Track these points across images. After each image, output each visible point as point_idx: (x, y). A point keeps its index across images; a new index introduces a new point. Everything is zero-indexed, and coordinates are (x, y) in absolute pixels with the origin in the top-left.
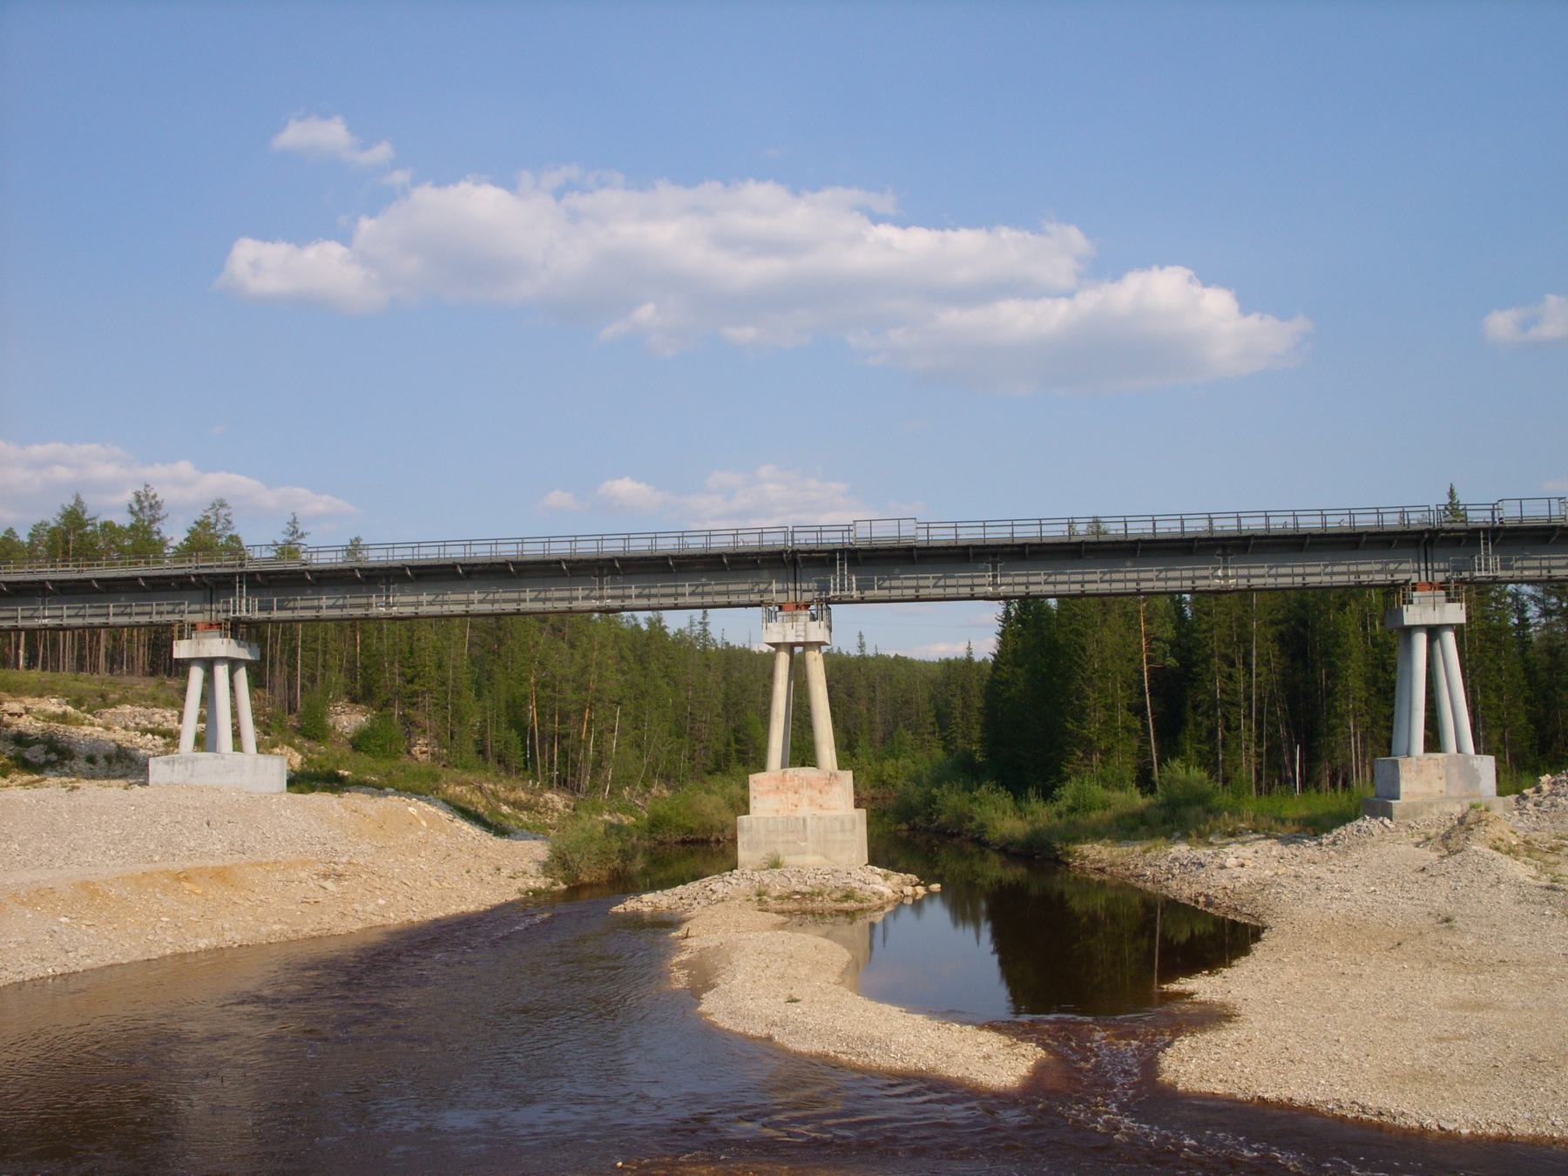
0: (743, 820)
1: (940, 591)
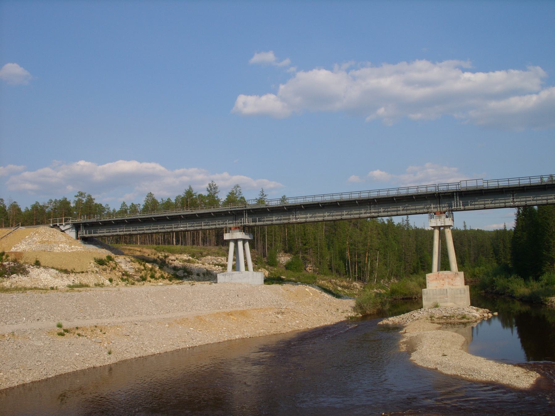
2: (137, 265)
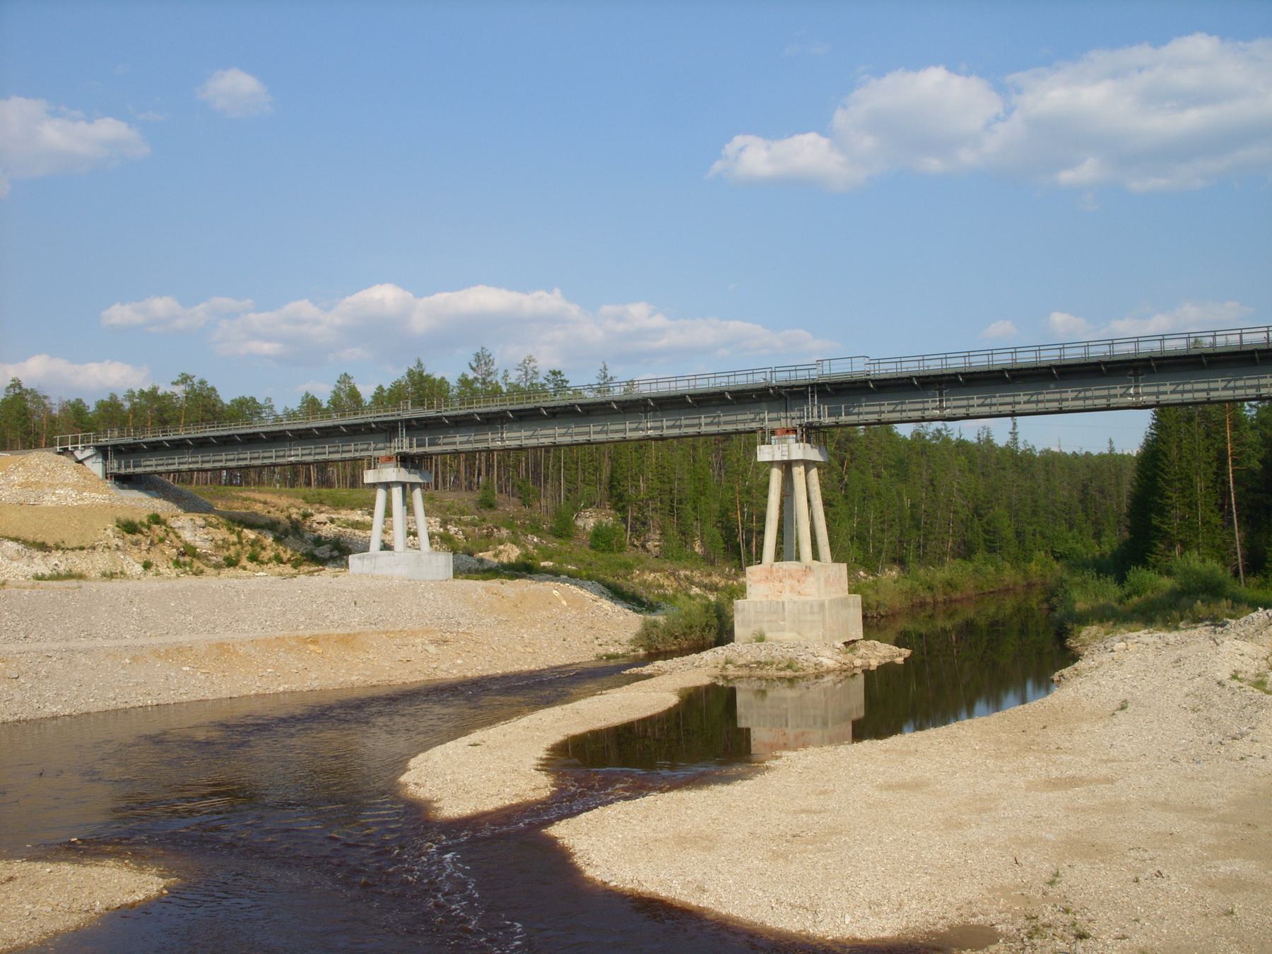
0: (739, 603)
1: (1080, 403)
2: (221, 534)
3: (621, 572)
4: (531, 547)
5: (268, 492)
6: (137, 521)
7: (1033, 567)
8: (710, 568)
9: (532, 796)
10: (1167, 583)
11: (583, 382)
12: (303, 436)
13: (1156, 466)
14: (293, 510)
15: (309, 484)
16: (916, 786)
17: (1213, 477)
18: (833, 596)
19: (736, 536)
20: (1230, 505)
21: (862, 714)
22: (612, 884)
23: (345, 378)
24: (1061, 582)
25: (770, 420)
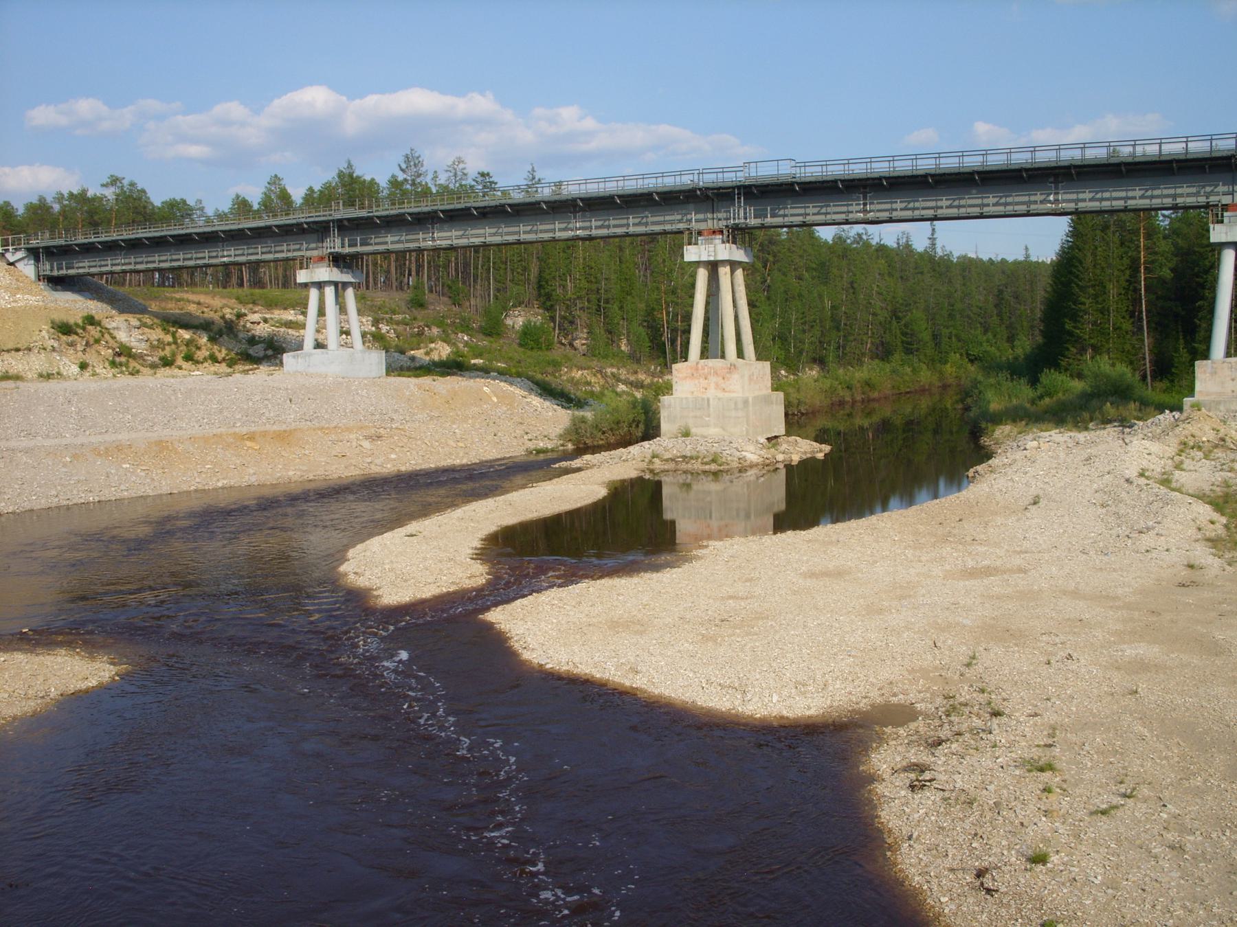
0: (665, 399)
2: (157, 334)
3: (550, 369)
4: (461, 345)
5: (201, 293)
6: (72, 321)
7: (948, 369)
8: (635, 366)
9: (468, 584)
10: (1078, 386)
11: (511, 183)
12: (236, 237)
13: (1071, 272)
14: (227, 311)
15: (241, 285)
16: (839, 574)
17: (1125, 284)
18: (757, 393)
19: (661, 335)
20: (1141, 312)
21: (783, 507)
22: (548, 666)
23: (276, 180)
24: (976, 383)
25: (697, 221)
